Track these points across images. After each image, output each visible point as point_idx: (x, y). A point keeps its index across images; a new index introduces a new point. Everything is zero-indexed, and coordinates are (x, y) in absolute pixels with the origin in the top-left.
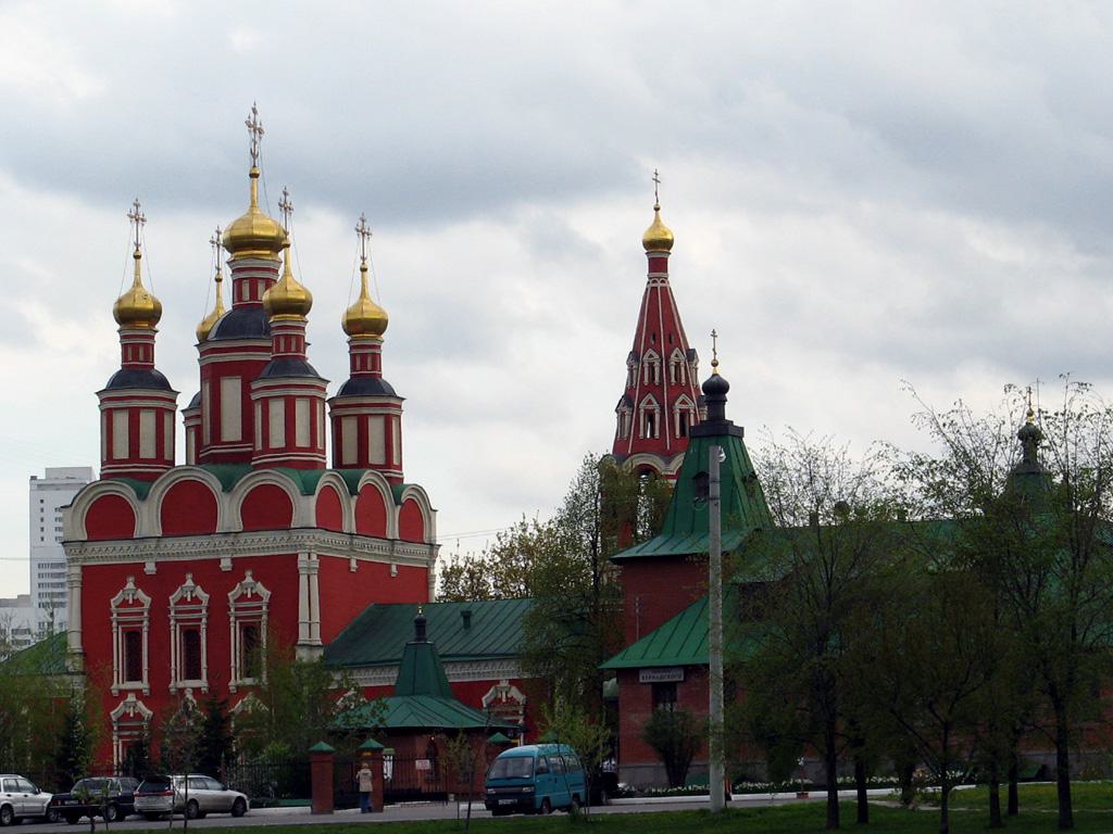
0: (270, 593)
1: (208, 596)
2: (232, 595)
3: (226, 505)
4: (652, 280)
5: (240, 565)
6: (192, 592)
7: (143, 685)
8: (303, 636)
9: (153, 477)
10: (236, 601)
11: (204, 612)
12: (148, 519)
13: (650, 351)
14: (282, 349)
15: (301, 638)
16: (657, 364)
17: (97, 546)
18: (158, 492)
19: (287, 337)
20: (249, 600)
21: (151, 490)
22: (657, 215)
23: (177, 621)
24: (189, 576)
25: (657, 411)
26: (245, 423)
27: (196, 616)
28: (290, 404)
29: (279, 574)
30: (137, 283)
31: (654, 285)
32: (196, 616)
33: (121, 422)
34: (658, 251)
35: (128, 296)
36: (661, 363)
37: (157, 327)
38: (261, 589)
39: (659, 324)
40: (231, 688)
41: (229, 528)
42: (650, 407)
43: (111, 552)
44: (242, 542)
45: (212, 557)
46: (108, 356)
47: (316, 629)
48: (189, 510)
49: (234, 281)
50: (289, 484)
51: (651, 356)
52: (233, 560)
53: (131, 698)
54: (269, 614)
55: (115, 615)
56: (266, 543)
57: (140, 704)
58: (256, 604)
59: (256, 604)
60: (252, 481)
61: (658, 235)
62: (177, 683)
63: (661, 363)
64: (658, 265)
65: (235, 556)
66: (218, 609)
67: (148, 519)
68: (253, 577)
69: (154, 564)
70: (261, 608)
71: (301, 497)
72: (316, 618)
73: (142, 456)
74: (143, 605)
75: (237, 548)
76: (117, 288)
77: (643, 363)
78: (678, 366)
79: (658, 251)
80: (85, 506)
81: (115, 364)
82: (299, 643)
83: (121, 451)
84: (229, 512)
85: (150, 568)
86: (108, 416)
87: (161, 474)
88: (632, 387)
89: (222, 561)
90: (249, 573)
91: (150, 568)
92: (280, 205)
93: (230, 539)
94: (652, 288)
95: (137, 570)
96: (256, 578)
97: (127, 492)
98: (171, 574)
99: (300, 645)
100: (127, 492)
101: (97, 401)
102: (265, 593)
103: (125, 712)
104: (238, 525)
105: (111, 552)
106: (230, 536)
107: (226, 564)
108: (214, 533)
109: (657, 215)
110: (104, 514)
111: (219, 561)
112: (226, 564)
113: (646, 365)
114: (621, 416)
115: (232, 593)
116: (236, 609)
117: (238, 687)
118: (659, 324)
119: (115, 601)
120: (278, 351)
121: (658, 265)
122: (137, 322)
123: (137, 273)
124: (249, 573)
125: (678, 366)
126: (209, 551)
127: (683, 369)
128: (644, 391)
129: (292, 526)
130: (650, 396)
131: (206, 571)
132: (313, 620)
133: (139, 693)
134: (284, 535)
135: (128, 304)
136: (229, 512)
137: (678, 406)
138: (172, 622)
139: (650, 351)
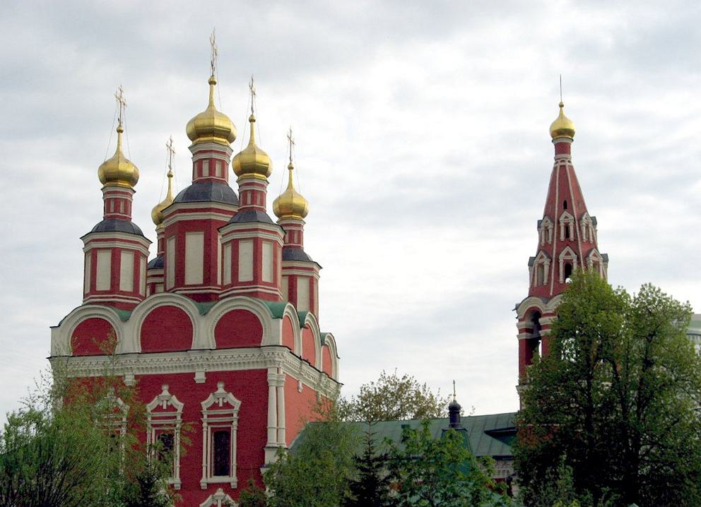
0: (183, 404)
1: (183, 404)
2: (205, 404)
5: (213, 378)
6: (223, 398)
7: (232, 479)
8: (272, 439)
9: (130, 307)
10: (208, 409)
15: (269, 441)
16: (571, 225)
18: (218, 311)
19: (253, 192)
20: (221, 408)
21: (212, 310)
22: (561, 110)
23: (209, 424)
25: (575, 260)
26: (203, 262)
27: (227, 419)
28: (257, 243)
31: (563, 164)
32: (227, 419)
33: (104, 260)
34: (562, 139)
35: (112, 160)
38: (231, 398)
39: (564, 194)
40: (202, 485)
41: (203, 346)
42: (568, 258)
43: (93, 366)
44: (216, 358)
45: (187, 371)
47: (283, 434)
48: (166, 331)
50: (260, 309)
51: (566, 217)
52: (207, 374)
53: (220, 492)
54: (239, 421)
55: (149, 419)
56: (238, 360)
57: (228, 497)
58: (227, 411)
59: (227, 411)
60: (234, 304)
62: (207, 479)
63: (575, 223)
65: (138, 373)
66: (192, 414)
67: (129, 335)
68: (170, 391)
70: (232, 415)
71: (271, 320)
72: (283, 425)
73: (122, 288)
74: (233, 408)
75: (211, 363)
77: (559, 222)
79: (562, 139)
80: (72, 327)
82: (268, 445)
83: (103, 283)
84: (204, 331)
85: (129, 380)
86: (92, 255)
88: (546, 243)
89: (196, 374)
90: (165, 388)
93: (206, 355)
94: (561, 166)
96: (227, 388)
98: (148, 386)
99: (269, 447)
100: (111, 315)
103: (213, 504)
104: (212, 344)
105: (93, 366)
106: (204, 355)
107: (200, 378)
109: (561, 110)
110: (88, 335)
111: (193, 375)
112: (200, 378)
113: (562, 224)
115: (206, 401)
116: (209, 416)
117: (208, 485)
118: (564, 194)
120: (245, 203)
122: (117, 182)
124: (165, 388)
125: (587, 227)
129: (262, 345)
130: (568, 249)
131: (183, 384)
132: (280, 426)
133: (226, 487)
134: (255, 351)
135: (111, 166)
136: (204, 331)
137: (562, 256)
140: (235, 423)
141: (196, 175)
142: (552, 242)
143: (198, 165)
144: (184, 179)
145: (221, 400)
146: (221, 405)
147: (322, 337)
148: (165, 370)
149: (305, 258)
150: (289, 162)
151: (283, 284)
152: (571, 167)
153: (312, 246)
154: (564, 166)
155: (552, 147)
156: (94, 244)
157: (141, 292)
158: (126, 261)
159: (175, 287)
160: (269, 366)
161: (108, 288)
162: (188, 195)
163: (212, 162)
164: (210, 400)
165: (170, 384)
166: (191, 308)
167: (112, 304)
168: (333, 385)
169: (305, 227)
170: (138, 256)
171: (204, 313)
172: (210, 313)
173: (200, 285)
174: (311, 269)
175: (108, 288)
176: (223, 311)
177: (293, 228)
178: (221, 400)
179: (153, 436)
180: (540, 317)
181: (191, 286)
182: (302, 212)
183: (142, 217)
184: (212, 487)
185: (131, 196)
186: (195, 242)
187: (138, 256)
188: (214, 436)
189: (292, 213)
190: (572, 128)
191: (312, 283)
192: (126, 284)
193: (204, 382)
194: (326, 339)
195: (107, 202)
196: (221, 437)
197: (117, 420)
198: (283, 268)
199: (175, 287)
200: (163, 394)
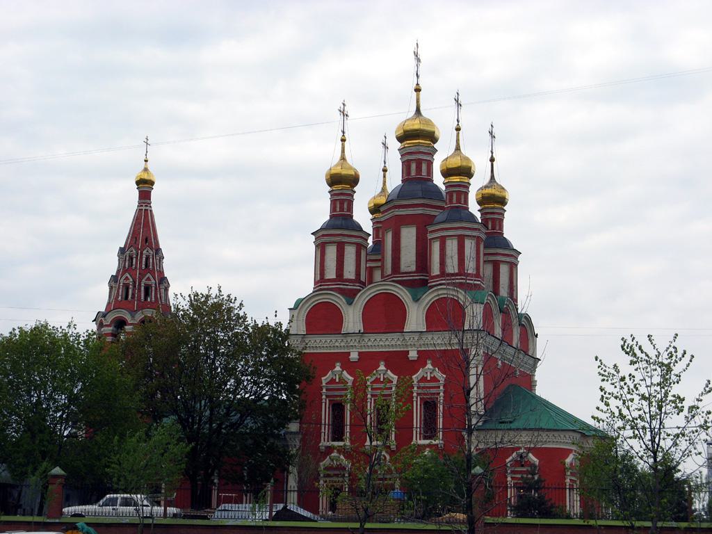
0: (397, 377)
1: (397, 377)
3: (351, 316)
4: (140, 205)
5: (424, 356)
11: (442, 388)
12: (353, 318)
13: (132, 248)
14: (338, 209)
17: (373, 337)
18: (429, 298)
20: (337, 383)
21: (424, 296)
24: (429, 362)
29: (455, 363)
30: (343, 158)
33: (331, 252)
34: (145, 187)
36: (137, 256)
37: (355, 189)
42: (149, 283)
45: (346, 351)
46: (320, 211)
48: (386, 314)
49: (403, 162)
52: (360, 354)
58: (341, 386)
61: (146, 177)
62: (325, 443)
64: (145, 196)
65: (420, 349)
66: (359, 388)
67: (353, 318)
69: (416, 352)
74: (392, 382)
76: (137, 173)
78: (147, 258)
79: (145, 187)
81: (325, 217)
83: (331, 274)
84: (416, 318)
85: (354, 356)
86: (321, 247)
87: (360, 290)
91: (354, 356)
92: (461, 105)
95: (343, 358)
97: (339, 301)
98: (369, 360)
101: (313, 238)
102: (395, 378)
104: (359, 327)
107: (413, 355)
108: (340, 334)
111: (349, 354)
112: (413, 355)
114: (111, 288)
115: (325, 378)
119: (325, 380)
121: (145, 196)
122: (342, 184)
123: (343, 151)
125: (147, 258)
126: (385, 345)
127: (151, 260)
128: (125, 271)
131: (398, 361)
136: (416, 318)
138: (324, 397)
139: (132, 248)
140: (442, 394)
141: (404, 175)
142: (136, 268)
143: (406, 165)
144: (395, 180)
145: (429, 374)
146: (429, 379)
147: (520, 316)
148: (366, 348)
149: (506, 244)
150: (383, 165)
151: (488, 271)
152: (151, 211)
153: (510, 231)
154: (147, 210)
155: (137, 193)
156: (323, 239)
157: (363, 279)
158: (350, 252)
159: (391, 275)
160: (410, 349)
161: (334, 276)
162: (402, 193)
163: (419, 163)
164: (420, 373)
165: (385, 361)
166: (404, 294)
167: (461, 286)
168: (531, 362)
169: (506, 214)
170: (360, 247)
171: (416, 299)
172: (354, 302)
173: (414, 272)
174: (512, 257)
175: (334, 276)
176: (365, 299)
177: (496, 216)
178: (429, 374)
179: (327, 404)
180: (126, 325)
181: (406, 273)
182: (502, 201)
183: (362, 217)
184: (329, 450)
185: (353, 196)
186: (409, 236)
187: (360, 247)
188: (332, 406)
189: (494, 202)
190: (153, 180)
191: (513, 266)
192: (349, 272)
193: (416, 359)
194: (523, 319)
195: (333, 203)
196: (430, 406)
197: (387, 389)
198: (485, 254)
199: (391, 275)
200: (335, 370)
